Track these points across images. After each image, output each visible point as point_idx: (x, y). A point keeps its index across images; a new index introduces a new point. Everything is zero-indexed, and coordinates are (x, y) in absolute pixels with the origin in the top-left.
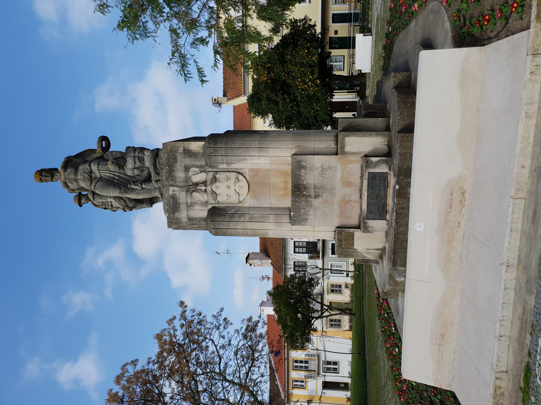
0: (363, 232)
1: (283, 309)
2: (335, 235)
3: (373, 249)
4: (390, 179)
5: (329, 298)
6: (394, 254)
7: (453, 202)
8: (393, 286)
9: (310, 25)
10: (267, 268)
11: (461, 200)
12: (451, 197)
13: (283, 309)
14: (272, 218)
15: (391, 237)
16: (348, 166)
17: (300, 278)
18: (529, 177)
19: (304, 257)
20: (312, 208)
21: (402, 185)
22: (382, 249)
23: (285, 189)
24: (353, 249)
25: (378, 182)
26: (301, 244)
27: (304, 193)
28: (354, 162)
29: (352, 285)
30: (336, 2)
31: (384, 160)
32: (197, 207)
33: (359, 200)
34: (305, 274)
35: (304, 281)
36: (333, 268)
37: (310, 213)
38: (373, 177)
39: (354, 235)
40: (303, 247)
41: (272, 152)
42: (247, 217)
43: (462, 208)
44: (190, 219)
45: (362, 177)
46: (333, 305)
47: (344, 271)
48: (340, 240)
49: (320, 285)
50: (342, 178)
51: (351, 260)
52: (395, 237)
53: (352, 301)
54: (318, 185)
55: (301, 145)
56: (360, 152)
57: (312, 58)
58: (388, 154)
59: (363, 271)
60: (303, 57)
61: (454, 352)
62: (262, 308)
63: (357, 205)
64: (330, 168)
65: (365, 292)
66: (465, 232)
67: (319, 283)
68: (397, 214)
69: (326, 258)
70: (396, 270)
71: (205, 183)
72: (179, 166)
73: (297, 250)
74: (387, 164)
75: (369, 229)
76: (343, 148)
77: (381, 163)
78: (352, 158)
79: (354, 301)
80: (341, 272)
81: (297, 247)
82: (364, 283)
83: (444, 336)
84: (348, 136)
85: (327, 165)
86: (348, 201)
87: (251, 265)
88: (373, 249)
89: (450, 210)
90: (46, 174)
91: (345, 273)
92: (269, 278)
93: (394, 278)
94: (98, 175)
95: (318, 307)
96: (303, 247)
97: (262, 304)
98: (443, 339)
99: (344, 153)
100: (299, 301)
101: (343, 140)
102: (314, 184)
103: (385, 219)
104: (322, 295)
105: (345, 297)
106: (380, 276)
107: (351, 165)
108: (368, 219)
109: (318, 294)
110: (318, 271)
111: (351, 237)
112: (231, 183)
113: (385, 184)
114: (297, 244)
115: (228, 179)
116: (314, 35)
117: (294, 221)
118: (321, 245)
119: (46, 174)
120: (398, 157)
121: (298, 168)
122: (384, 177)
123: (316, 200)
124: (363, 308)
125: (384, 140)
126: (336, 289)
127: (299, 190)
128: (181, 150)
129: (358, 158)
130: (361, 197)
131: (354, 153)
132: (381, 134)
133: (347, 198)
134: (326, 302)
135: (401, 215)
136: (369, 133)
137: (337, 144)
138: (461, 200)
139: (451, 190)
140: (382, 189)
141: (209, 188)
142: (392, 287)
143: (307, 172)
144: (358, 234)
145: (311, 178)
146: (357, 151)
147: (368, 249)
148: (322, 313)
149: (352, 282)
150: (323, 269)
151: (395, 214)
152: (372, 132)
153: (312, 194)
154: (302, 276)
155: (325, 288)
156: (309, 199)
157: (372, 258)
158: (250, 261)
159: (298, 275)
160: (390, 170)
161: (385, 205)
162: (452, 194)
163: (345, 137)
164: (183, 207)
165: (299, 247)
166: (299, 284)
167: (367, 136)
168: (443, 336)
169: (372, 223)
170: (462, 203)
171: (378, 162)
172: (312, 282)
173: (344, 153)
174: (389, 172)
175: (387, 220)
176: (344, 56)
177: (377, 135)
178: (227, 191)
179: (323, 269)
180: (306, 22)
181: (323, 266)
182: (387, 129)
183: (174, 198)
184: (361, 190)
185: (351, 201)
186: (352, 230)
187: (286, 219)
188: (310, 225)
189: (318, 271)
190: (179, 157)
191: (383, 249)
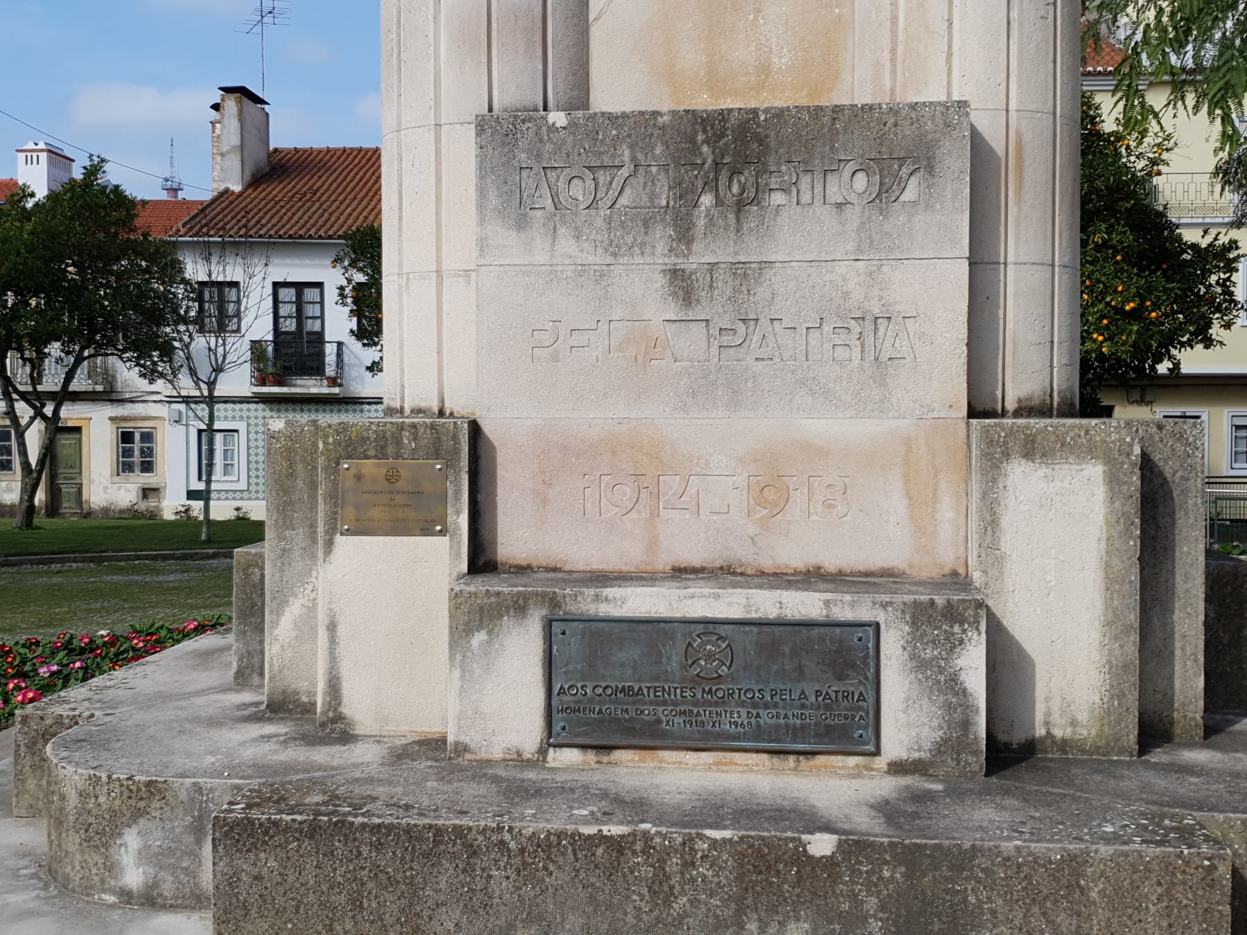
0: (455, 596)
1: (29, 227)
2: (417, 411)
3: (333, 659)
4: (833, 772)
5: (98, 428)
8: (82, 811)
9: (1209, 324)
10: (210, 175)
13: (29, 227)
15: (430, 798)
17: (169, 300)
19: (257, 323)
20: (599, 258)
21: (834, 878)
22: (339, 718)
24: (331, 531)
25: (810, 688)
26: (312, 310)
27: (707, 200)
29: (153, 515)
30: (1238, 428)
31: (966, 724)
33: (663, 562)
34: (185, 320)
35: (156, 318)
36: (219, 437)
37: (567, 245)
38: (843, 657)
39: (426, 531)
40: (300, 316)
45: (811, 578)
46: (65, 441)
47: (209, 482)
48: (386, 443)
49: (143, 384)
51: (257, 510)
52: (439, 831)
53: (88, 514)
54: (762, 292)
55: (1029, 173)
56: (1000, 561)
57: (1099, 330)
58: (1010, 754)
59: (214, 556)
60: (1103, 294)
62: (44, 157)
63: (627, 554)
64: (882, 367)
65: (121, 570)
67: (152, 381)
68: (617, 846)
69: (260, 410)
70: (197, 830)
73: (287, 294)
74: (941, 747)
75: (479, 638)
76: (1031, 450)
77: (949, 707)
78: (947, 514)
79: (85, 523)
80: (206, 468)
81: (299, 295)
82: (160, 564)
84: (1113, 481)
85: (903, 348)
87: (216, 107)
88: (333, 659)
91: (201, 486)
95: (52, 381)
96: (300, 316)
97: (58, 158)
100: (75, 296)
101: (1090, 451)
102: (764, 265)
103: (552, 738)
104: (108, 394)
105: (104, 487)
106: (164, 698)
107: (897, 504)
108: (548, 625)
109: (109, 378)
110: (204, 372)
113: (797, 733)
114: (311, 294)
116: (1170, 340)
117: (502, 133)
118: (314, 390)
120: (1052, 849)
121: (889, 147)
123: (660, 281)
124: (51, 561)
125: (1083, 717)
126: (135, 450)
127: (728, 158)
129: (947, 543)
130: (681, 573)
131: (991, 524)
132: (1121, 696)
133: (672, 483)
134: (70, 413)
135: (612, 871)
136: (1133, 617)
137: (1025, 410)
140: (766, 718)
142: (73, 800)
143: (854, 215)
144: (438, 557)
145: (807, 238)
146: (1010, 541)
147: (332, 627)
148: (24, 396)
149: (168, 515)
150: (211, 400)
151: (615, 830)
152: (1135, 637)
153: (701, 256)
154: (175, 311)
155: (138, 409)
156: (661, 236)
157: (272, 651)
158: (231, 105)
159: (180, 291)
160: (897, 768)
161: (650, 737)
163: (1109, 461)
165: (299, 303)
166: (143, 295)
167: (1108, 601)
169: (520, 651)
171: (953, 685)
172: (152, 349)
173: (994, 458)
174: (881, 763)
175: (542, 751)
177: (1116, 671)
179: (211, 400)
180: (1218, 309)
181: (226, 400)
182: (1154, 732)
184: (726, 574)
185: (655, 514)
186: (463, 520)
187: (515, 85)
188: (482, 244)
189: (204, 372)
191: (336, 729)
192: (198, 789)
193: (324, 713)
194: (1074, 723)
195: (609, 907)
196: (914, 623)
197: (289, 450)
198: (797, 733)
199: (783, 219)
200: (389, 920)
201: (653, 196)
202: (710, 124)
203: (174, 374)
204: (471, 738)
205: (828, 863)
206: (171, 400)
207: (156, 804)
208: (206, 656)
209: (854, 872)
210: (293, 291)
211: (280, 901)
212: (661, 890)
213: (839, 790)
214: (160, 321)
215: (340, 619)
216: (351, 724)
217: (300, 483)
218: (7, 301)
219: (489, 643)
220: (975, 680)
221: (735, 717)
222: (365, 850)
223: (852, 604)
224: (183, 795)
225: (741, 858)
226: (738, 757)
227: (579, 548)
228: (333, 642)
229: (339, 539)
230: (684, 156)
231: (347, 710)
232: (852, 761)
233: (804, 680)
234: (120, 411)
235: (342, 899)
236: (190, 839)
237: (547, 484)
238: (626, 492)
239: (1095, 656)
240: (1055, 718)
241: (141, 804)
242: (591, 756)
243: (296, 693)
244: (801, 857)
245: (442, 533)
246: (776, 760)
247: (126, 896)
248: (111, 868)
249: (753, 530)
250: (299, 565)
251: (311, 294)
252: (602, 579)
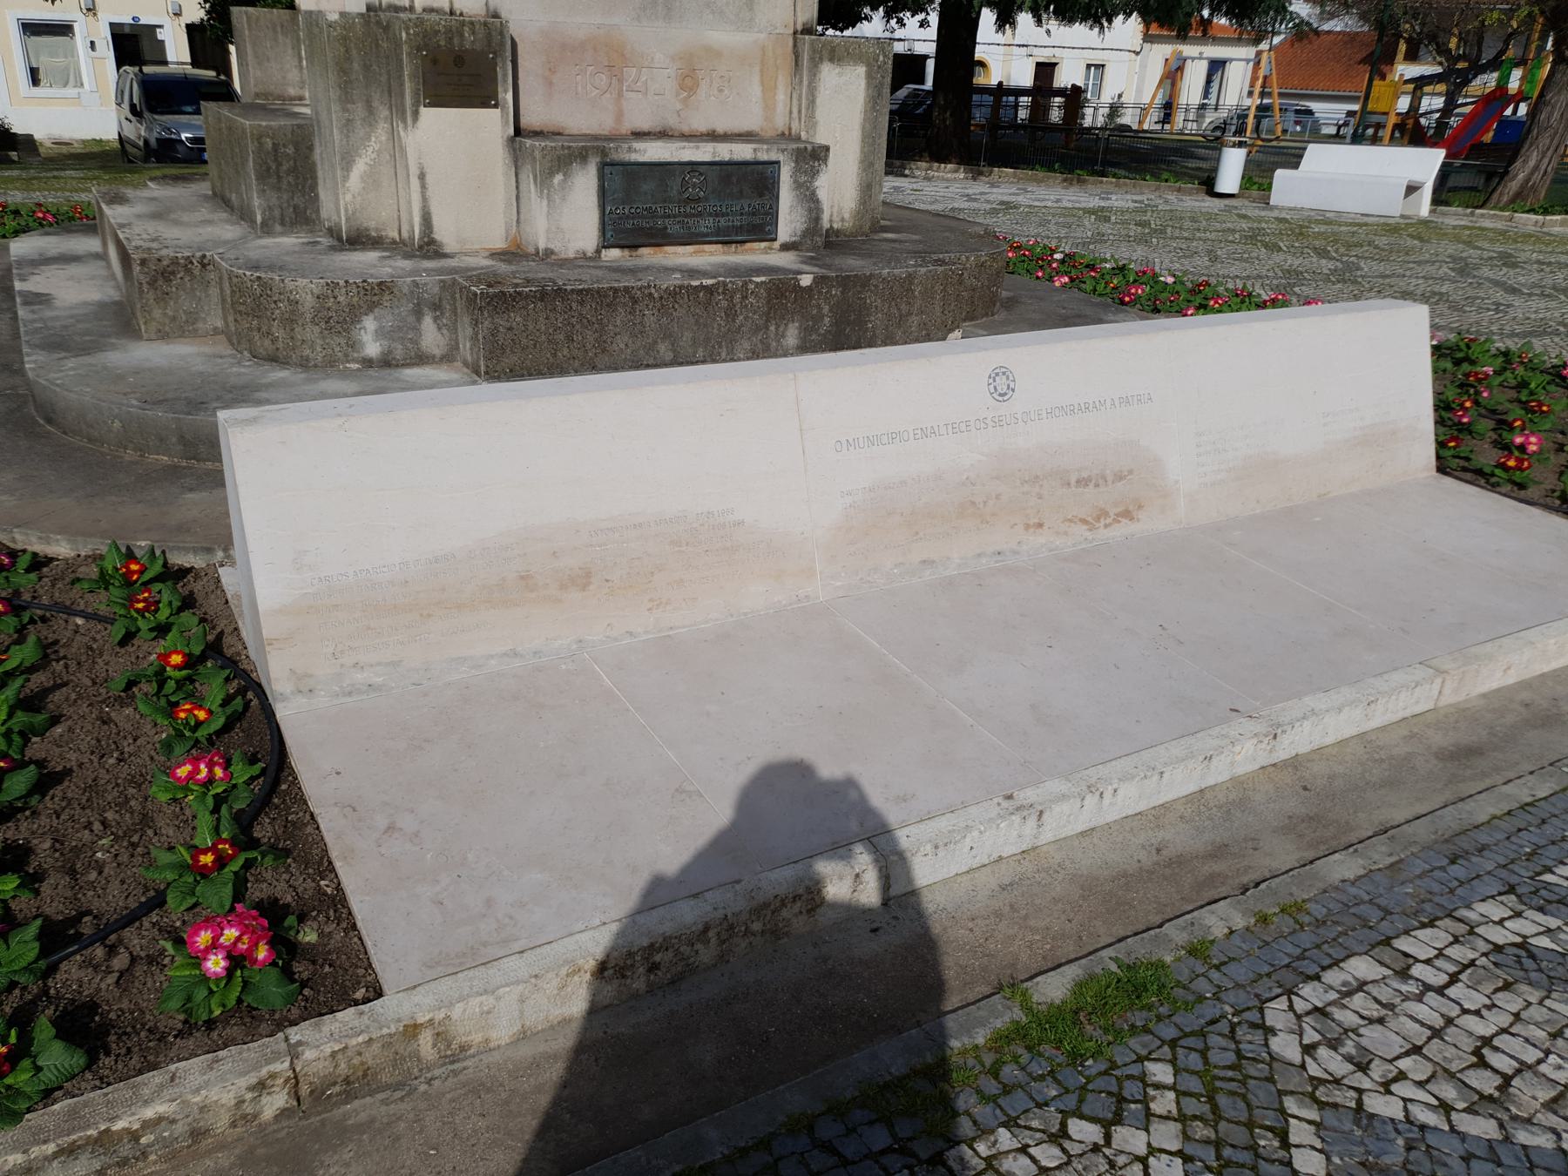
3: (424, 199)
6: (543, 295)
7: (1097, 485)
11: (1106, 514)
12: (1110, 479)
16: (756, 79)
18: (1484, 696)
22: (432, 242)
24: (416, 105)
28: (769, 106)
43: (1084, 521)
50: (714, 53)
52: (616, 290)
61: (515, 654)
66: (1015, 553)
68: (709, 290)
75: (558, 178)
77: (810, 210)
78: (781, 96)
83: (584, 587)
84: (869, 76)
86: (621, 81)
88: (424, 199)
89: (1073, 482)
93: (372, 307)
98: (563, 587)
103: (605, 244)
107: (756, 90)
122: (761, 228)
125: (847, 216)
138: (1106, 514)
139: (1131, 472)
146: (821, 113)
147: (422, 177)
160: (785, 247)
161: (660, 239)
162: (1119, 477)
163: (868, 65)
167: (863, 147)
168: (582, 580)
169: (583, 187)
170: (1098, 519)
174: (776, 245)
175: (598, 251)
176: (1089, 66)
184: (713, 136)
185: (620, 95)
186: (510, 96)
192: (415, 284)
193: (421, 239)
194: (843, 220)
195: (705, 326)
196: (796, 162)
197: (345, 38)
198: (738, 230)
200: (589, 346)
204: (556, 246)
205: (809, 288)
207: (387, 297)
209: (820, 293)
211: (524, 341)
212: (731, 314)
215: (427, 170)
216: (440, 245)
217: (356, 66)
218: (1522, 79)
219: (565, 181)
221: (705, 225)
222: (574, 305)
223: (768, 150)
224: (406, 290)
225: (769, 291)
226: (706, 247)
228: (423, 187)
229: (423, 110)
231: (437, 236)
232: (763, 245)
235: (562, 337)
236: (411, 319)
237: (552, 71)
238: (603, 79)
240: (835, 218)
241: (375, 298)
242: (626, 252)
243: (367, 229)
244: (797, 288)
245: (496, 106)
246: (726, 248)
247: (368, 363)
248: (353, 345)
249: (679, 106)
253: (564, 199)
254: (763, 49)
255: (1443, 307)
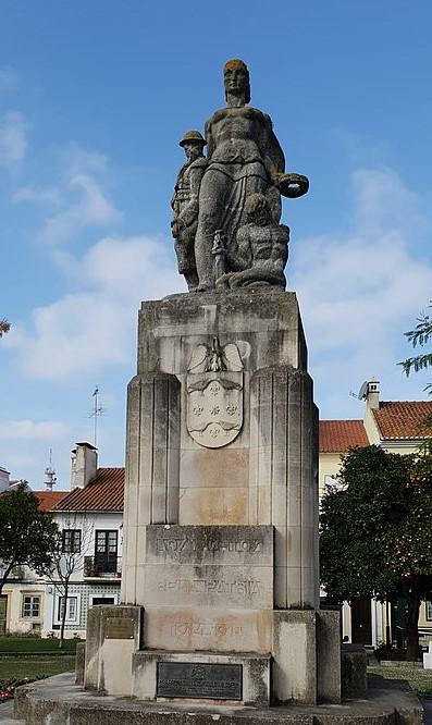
0: (134, 655)
14: (159, 490)
16: (255, 628)
19: (88, 549)
23: (213, 516)
26: (112, 543)
28: (261, 638)
32: (179, 354)
33: (192, 649)
34: (58, 550)
37: (169, 560)
41: (279, 489)
42: (162, 446)
44: (158, 342)
45: (233, 653)
47: (64, 621)
48: (119, 613)
49: (38, 577)
51: (83, 634)
53: (9, 635)
56: (279, 650)
58: (275, 701)
59: (65, 654)
63: (184, 646)
64: (251, 595)
71: (223, 368)
72: (254, 323)
73: (103, 535)
75: (140, 667)
81: (107, 535)
84: (308, 628)
86: (191, 629)
87: (74, 452)
90: (239, 82)
92: (50, 484)
94: (237, 176)
96: (107, 546)
99: (277, 621)
104: (21, 581)
109: (21, 573)
111: (126, 634)
112: (223, 416)
114: (112, 535)
115: (231, 410)
117: (154, 529)
119: (239, 82)
121: (252, 537)
126: (31, 606)
127: (211, 538)
128: (283, 326)
137: (293, 608)
141: (214, 376)
143: (243, 554)
144: (131, 646)
145: (231, 560)
149: (44, 636)
153: (204, 563)
155: (34, 587)
156: (194, 557)
158: (81, 451)
159: (56, 537)
160: (246, 704)
161: (184, 695)
164: (180, 329)
165: (107, 539)
166: (41, 539)
169: (150, 670)
172: (42, 562)
173: (277, 621)
174: (243, 703)
178: (209, 409)
181: (73, 583)
182: (322, 700)
183: (197, 313)
184: (210, 651)
190: (269, 322)
191: (103, 692)
199: (225, 555)
201: (192, 548)
202: (207, 529)
203: (51, 572)
204: (137, 694)
206: (48, 583)
208: (67, 678)
210: (104, 534)
213: (228, 708)
214: (47, 549)
220: (267, 682)
227: (170, 644)
230: (199, 537)
233: (224, 680)
234: (25, 588)
237: (162, 625)
238: (183, 629)
239: (305, 676)
250: (95, 647)
251: (112, 535)
252: (175, 652)
253: (142, 675)
254: (258, 617)
255: (257, 123)
